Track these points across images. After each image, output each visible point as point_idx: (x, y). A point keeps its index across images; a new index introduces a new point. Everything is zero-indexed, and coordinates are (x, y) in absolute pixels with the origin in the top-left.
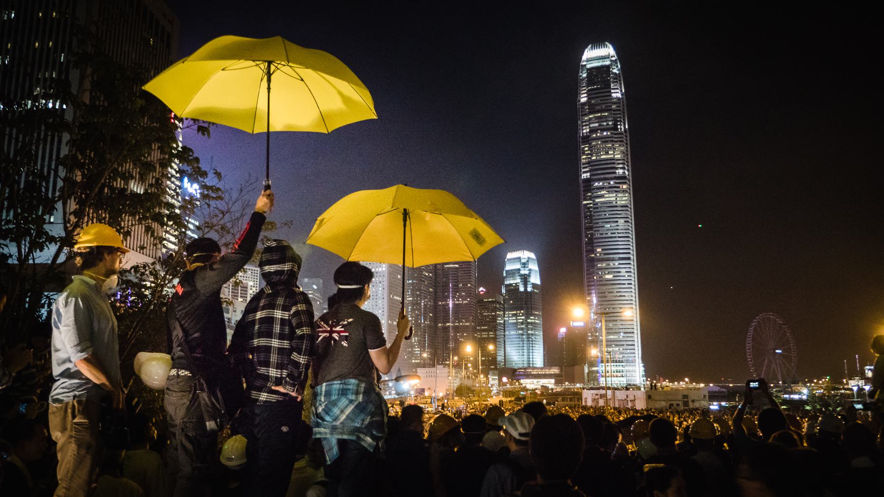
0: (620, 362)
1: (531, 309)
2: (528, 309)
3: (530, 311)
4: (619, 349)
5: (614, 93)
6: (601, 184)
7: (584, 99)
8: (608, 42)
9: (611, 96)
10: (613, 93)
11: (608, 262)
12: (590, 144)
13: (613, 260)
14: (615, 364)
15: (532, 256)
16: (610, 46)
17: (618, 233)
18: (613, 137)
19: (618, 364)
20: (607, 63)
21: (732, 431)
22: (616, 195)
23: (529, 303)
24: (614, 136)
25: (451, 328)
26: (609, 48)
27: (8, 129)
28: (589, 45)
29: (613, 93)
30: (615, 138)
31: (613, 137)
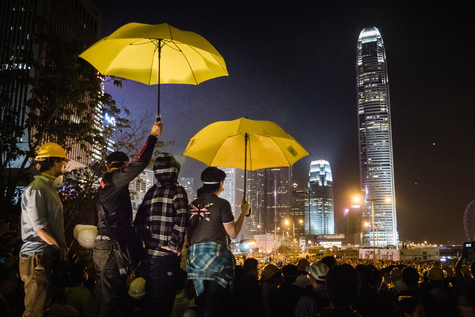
0: (383, 231)
1: (327, 197)
2: (324, 197)
5: (379, 59)
7: (360, 63)
10: (378, 59)
11: (376, 167)
12: (364, 92)
13: (379, 166)
16: (377, 29)
17: (382, 149)
18: (378, 87)
19: (382, 232)
20: (375, 40)
22: (381, 124)
26: (376, 30)
29: (378, 59)
30: (380, 88)
31: (378, 87)
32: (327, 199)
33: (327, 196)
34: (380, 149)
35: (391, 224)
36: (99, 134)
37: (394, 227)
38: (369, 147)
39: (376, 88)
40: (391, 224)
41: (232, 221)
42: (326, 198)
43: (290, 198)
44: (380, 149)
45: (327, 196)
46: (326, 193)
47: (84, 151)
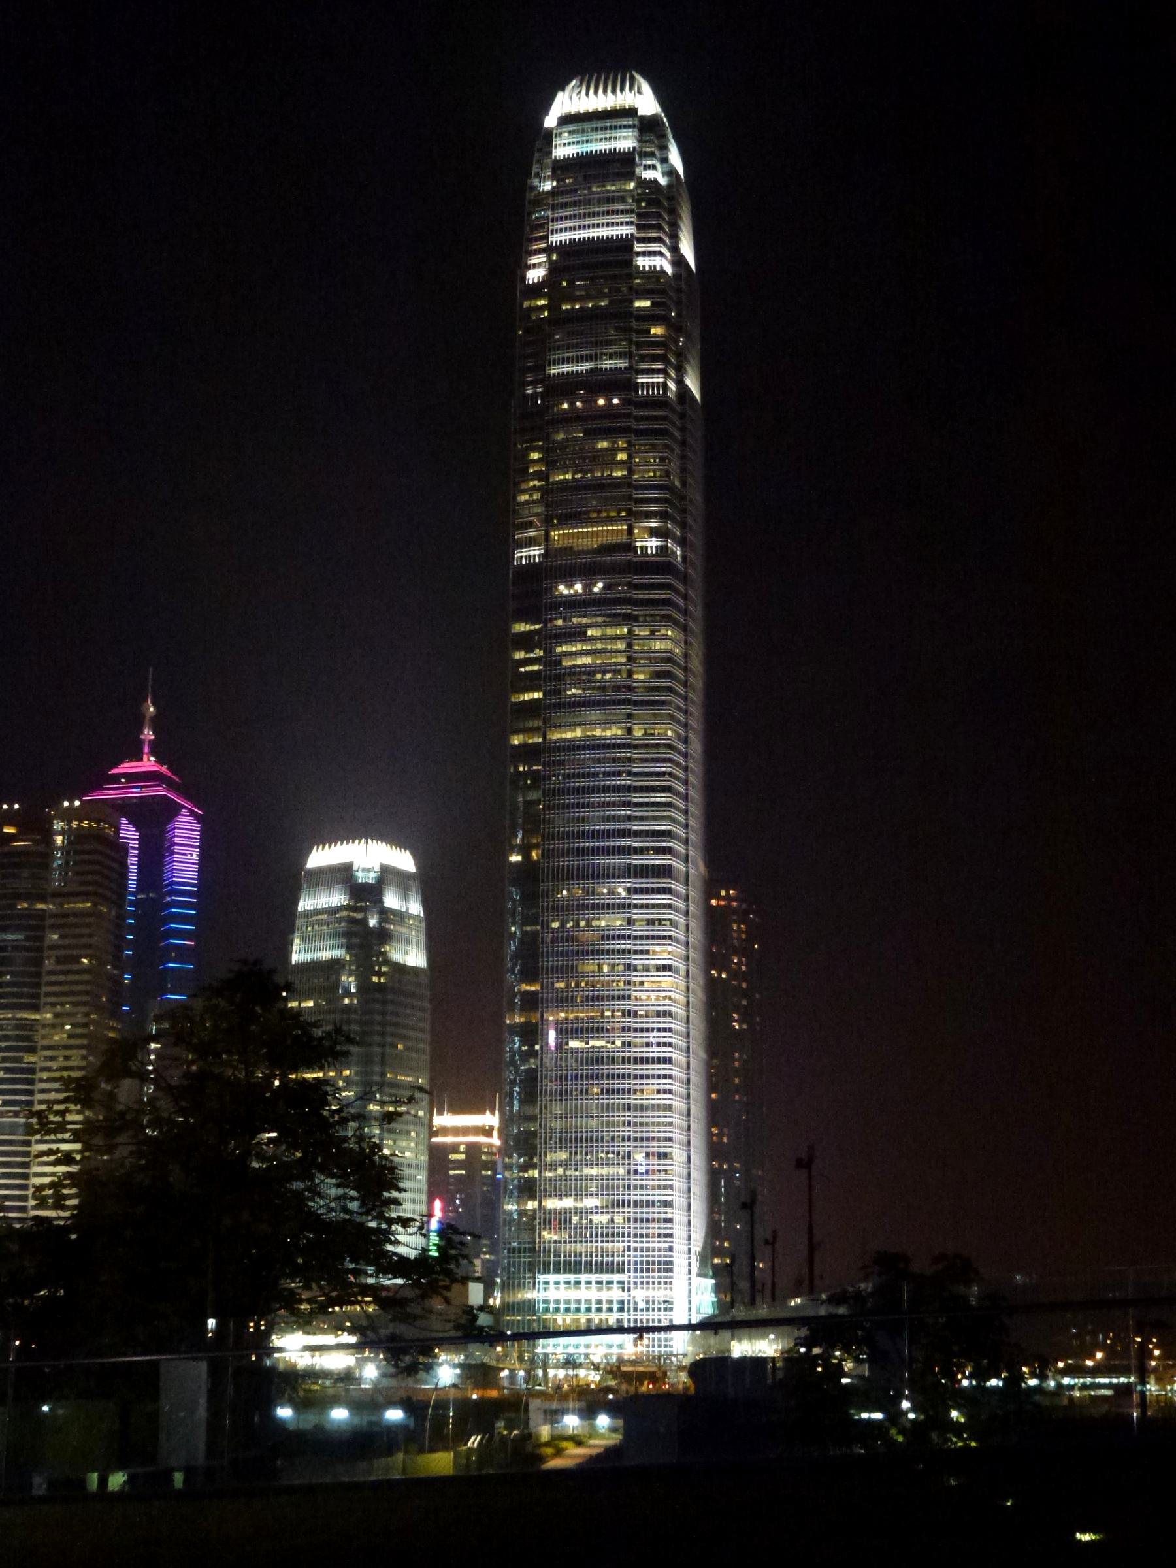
0: (610, 1268)
1: (383, 1063)
2: (367, 1060)
3: (377, 1069)
4: (612, 1221)
5: (644, 254)
6: (578, 587)
7: (534, 275)
8: (637, 72)
9: (629, 263)
10: (639, 254)
11: (590, 884)
12: (547, 438)
13: (609, 874)
14: (594, 1277)
15: (404, 861)
16: (646, 87)
17: (629, 773)
18: (629, 415)
19: (605, 1277)
20: (625, 141)
21: (286, 999)
22: (630, 631)
23: (377, 1039)
24: (636, 412)
25: (37, 991)
26: (640, 92)
27: (661, 392)
28: (571, 81)
29: (639, 254)
30: (638, 419)
31: (629, 415)
32: (383, 1074)
33: (383, 1055)
34: (619, 774)
35: (663, 1228)
36: (1026, 1383)
37: (679, 1245)
38: (562, 763)
39: (615, 416)
40: (663, 1228)
41: (161, 1028)
42: (377, 1069)
43: (677, 764)
44: (619, 774)
45: (383, 1055)
46: (378, 1028)
47: (61, 1079)
